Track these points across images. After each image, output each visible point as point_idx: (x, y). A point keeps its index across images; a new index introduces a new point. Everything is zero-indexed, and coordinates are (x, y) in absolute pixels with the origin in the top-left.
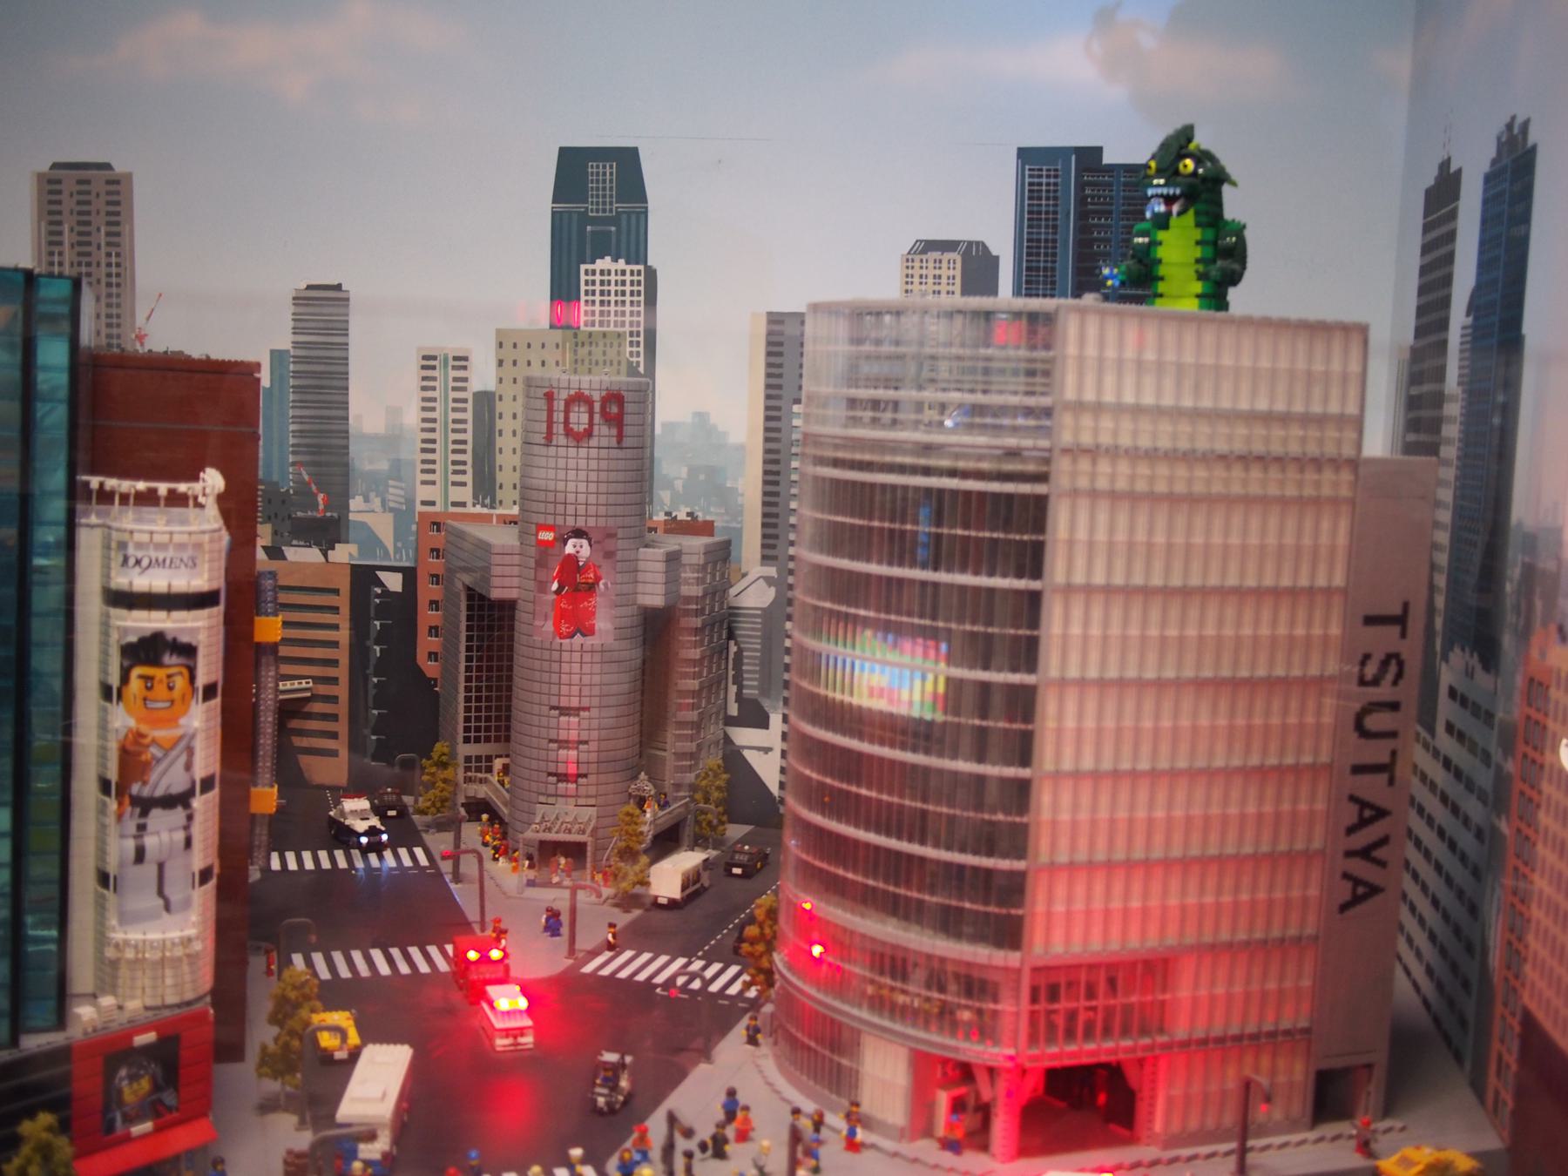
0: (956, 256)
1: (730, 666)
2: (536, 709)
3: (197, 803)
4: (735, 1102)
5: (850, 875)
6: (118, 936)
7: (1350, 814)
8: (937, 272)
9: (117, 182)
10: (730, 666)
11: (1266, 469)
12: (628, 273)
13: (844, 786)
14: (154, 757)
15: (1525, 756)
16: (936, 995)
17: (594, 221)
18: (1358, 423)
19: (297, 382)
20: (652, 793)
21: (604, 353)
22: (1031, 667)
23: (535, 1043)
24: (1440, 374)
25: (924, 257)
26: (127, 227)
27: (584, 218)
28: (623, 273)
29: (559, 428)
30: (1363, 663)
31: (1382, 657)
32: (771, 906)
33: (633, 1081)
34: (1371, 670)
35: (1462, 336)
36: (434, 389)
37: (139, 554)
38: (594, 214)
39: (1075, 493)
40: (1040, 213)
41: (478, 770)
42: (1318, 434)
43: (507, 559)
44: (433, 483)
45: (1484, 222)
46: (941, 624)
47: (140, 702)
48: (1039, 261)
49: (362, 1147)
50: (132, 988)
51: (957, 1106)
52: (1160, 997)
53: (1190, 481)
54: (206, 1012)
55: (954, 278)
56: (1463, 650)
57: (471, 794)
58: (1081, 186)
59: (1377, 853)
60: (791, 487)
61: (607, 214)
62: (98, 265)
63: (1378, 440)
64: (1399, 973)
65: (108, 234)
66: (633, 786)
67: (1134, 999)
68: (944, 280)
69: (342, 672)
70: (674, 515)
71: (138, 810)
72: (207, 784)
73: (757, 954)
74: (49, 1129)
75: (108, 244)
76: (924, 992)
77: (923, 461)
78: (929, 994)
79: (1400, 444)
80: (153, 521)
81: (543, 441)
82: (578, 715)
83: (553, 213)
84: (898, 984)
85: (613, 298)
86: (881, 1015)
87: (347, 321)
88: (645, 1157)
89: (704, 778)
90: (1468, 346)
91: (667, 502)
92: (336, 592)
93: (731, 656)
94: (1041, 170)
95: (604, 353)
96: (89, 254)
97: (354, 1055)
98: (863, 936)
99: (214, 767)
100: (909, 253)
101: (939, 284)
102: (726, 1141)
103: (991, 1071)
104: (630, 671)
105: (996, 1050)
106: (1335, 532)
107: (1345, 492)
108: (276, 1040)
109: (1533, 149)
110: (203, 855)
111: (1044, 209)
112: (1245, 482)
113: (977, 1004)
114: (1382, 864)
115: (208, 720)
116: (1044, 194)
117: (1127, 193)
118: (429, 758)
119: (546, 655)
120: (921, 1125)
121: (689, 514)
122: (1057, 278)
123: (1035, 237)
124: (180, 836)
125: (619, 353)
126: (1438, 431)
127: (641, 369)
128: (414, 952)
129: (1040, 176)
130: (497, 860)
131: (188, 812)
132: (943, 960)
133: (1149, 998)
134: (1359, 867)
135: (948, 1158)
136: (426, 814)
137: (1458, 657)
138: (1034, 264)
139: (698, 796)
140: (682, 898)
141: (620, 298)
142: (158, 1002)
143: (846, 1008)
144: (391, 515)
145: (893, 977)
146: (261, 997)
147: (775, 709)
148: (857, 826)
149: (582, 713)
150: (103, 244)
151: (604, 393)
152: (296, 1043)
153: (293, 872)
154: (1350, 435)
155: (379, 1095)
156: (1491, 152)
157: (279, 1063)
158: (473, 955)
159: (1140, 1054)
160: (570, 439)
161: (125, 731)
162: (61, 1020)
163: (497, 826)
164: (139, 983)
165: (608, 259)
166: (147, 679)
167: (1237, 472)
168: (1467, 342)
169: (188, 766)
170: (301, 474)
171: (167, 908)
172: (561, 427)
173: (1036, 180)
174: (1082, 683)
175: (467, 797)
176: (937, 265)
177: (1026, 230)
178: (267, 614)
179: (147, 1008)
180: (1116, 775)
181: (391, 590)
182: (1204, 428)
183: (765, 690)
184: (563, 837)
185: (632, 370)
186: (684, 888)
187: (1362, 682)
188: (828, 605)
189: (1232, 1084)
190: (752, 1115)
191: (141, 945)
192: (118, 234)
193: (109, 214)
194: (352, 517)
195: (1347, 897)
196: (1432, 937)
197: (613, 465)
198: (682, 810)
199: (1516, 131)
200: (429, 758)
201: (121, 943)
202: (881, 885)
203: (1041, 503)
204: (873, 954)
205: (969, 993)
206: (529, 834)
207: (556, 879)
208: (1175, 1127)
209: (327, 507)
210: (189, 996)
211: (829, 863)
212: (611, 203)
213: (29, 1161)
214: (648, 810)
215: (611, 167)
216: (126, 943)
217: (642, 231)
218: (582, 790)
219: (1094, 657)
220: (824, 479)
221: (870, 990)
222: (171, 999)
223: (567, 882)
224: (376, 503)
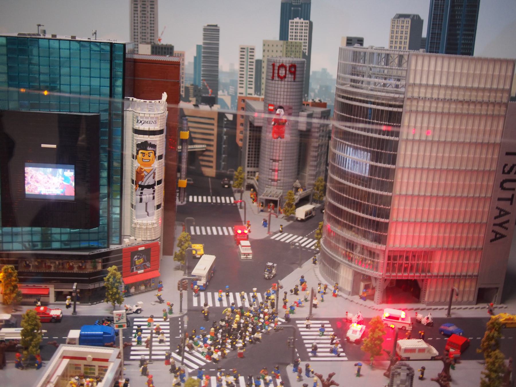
0: (409, 20)
3: (156, 187)
6: (136, 221)
8: (403, 25)
17: (294, 6)
22: (394, 163)
28: (302, 23)
29: (276, 75)
30: (504, 167)
31: (512, 165)
34: (507, 169)
41: (251, 175)
43: (259, 121)
44: (242, 87)
47: (141, 160)
49: (198, 282)
51: (367, 287)
52: (429, 262)
59: (506, 225)
65: (151, 8)
68: (405, 27)
69: (214, 143)
72: (159, 182)
74: (115, 270)
85: (299, 31)
91: (313, 96)
92: (213, 119)
96: (145, 14)
102: (298, 290)
103: (376, 279)
114: (506, 229)
118: (237, 171)
120: (355, 291)
124: (152, 196)
125: (300, 49)
127: (307, 54)
135: (361, 301)
139: (315, 188)
143: (337, 256)
157: (180, 258)
158: (239, 232)
165: (298, 18)
167: (466, 106)
169: (154, 178)
171: (148, 215)
185: (304, 55)
186: (306, 216)
190: (307, 284)
194: (219, 97)
197: (292, 87)
200: (237, 171)
202: (348, 223)
205: (370, 256)
206: (261, 197)
208: (431, 300)
209: (212, 93)
210: (154, 238)
213: (110, 278)
218: (279, 184)
220: (340, 102)
224: (226, 93)
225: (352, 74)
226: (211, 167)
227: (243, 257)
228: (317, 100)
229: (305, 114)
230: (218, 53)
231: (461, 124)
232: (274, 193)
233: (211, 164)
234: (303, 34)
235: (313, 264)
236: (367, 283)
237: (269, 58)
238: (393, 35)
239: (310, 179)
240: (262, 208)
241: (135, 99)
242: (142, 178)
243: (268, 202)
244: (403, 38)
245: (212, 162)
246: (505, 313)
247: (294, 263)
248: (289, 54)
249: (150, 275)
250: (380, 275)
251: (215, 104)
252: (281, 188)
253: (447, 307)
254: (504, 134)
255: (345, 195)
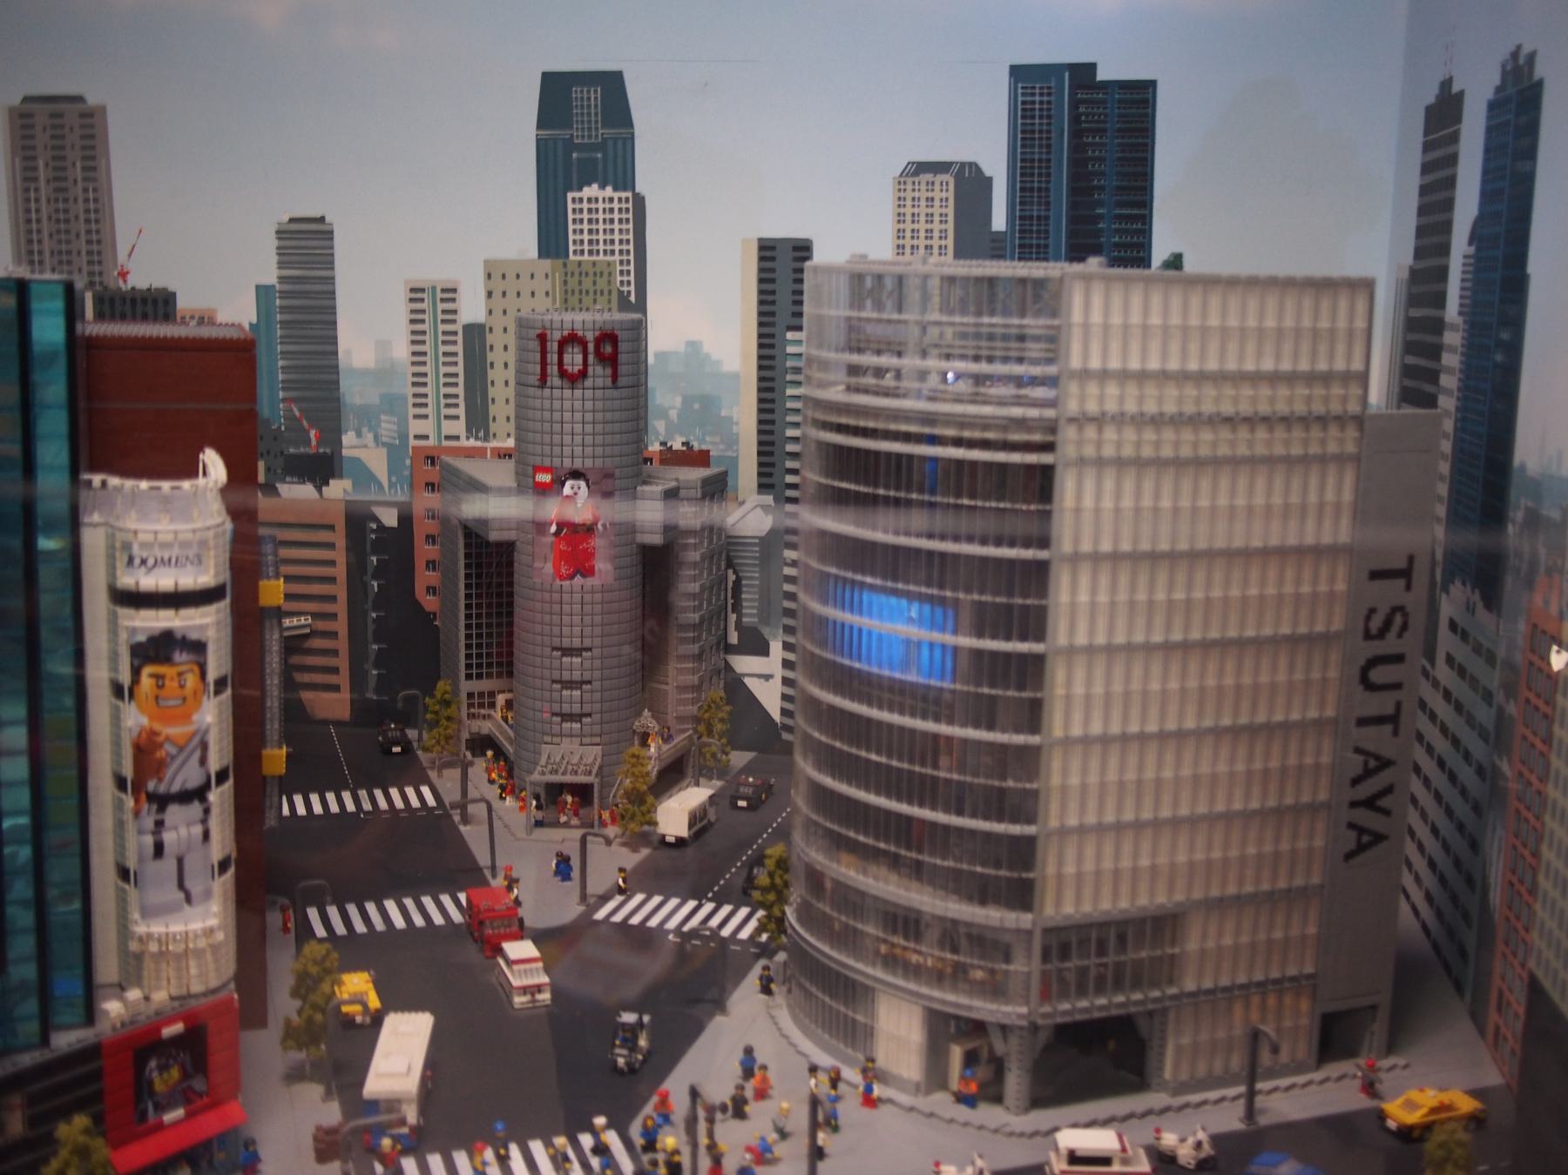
0: (948, 178)
1: (729, 595)
2: (538, 650)
3: (213, 797)
4: (753, 1060)
5: (861, 838)
6: (141, 929)
7: (1356, 764)
8: (930, 194)
9: (91, 115)
10: (729, 595)
11: (1271, 430)
12: (616, 200)
13: (854, 751)
14: (168, 754)
15: (1528, 701)
16: (949, 956)
18: (1363, 378)
19: (287, 317)
20: (656, 729)
21: (595, 283)
23: (553, 999)
24: (1440, 300)
25: (917, 179)
26: (104, 161)
27: (569, 145)
28: (611, 200)
29: (553, 369)
30: (1368, 618)
32: (781, 857)
33: (651, 1040)
34: (1376, 623)
35: (1464, 265)
36: (423, 321)
37: (145, 555)
38: (580, 141)
39: (1082, 462)
40: (1033, 132)
41: (481, 706)
42: (1323, 392)
44: (426, 417)
45: (1488, 151)
46: (949, 594)
48: (1033, 153)
50: (158, 978)
51: (970, 1059)
52: (1169, 951)
53: (1195, 445)
54: (233, 998)
55: (947, 199)
56: (1464, 584)
57: (475, 729)
58: (1075, 104)
59: (1384, 802)
60: (786, 415)
61: (593, 141)
62: (76, 200)
63: (1378, 392)
64: (1404, 907)
65: (84, 169)
66: (637, 723)
67: (1144, 954)
68: (937, 203)
69: (341, 608)
70: (669, 445)
71: (155, 807)
72: (222, 777)
73: (768, 903)
74: (86, 1131)
75: (85, 179)
76: (937, 953)
77: (927, 430)
78: (943, 955)
79: (1397, 390)
80: (158, 521)
81: (537, 383)
82: (581, 655)
83: (538, 141)
84: (912, 945)
85: (601, 227)
86: (894, 974)
87: (332, 255)
88: (666, 1118)
89: (706, 711)
90: (1471, 269)
91: (663, 432)
92: (331, 527)
93: (730, 585)
94: (1034, 88)
95: (595, 283)
97: (377, 1020)
98: (876, 898)
99: (228, 759)
100: (901, 175)
101: (932, 206)
102: (745, 1102)
103: (1004, 1029)
104: (632, 588)
105: (1008, 1009)
106: (1341, 488)
107: (1350, 448)
108: (300, 1013)
109: (1540, 83)
110: (222, 842)
111: (1037, 128)
112: (1250, 444)
113: (990, 965)
114: (1386, 812)
115: (220, 713)
116: (1037, 113)
117: (1122, 111)
118: (433, 696)
119: (547, 596)
120: (935, 1077)
121: (683, 444)
122: (1052, 199)
123: (1028, 157)
124: (197, 830)
126: (1438, 358)
127: (632, 298)
128: (427, 901)
129: (1033, 95)
130: (505, 799)
131: (205, 805)
132: (955, 922)
133: (1159, 952)
134: (1365, 817)
135: (963, 1112)
136: (432, 752)
137: (1457, 589)
138: (1028, 185)
139: (702, 728)
140: (690, 836)
141: (608, 227)
142: (184, 992)
143: (860, 966)
144: (384, 451)
145: (906, 938)
146: (283, 967)
147: (775, 637)
148: (867, 789)
149: (584, 654)
150: (79, 179)
151: (597, 333)
152: (319, 1017)
153: (302, 817)
154: (1355, 391)
155: (404, 1069)
156: (1495, 79)
159: (1150, 1006)
160: (565, 380)
161: (138, 729)
162: (90, 1014)
163: (502, 763)
164: (164, 974)
165: (595, 186)
166: (158, 677)
168: (1470, 265)
169: (203, 761)
170: (292, 410)
171: (188, 899)
172: (556, 368)
173: (1029, 99)
174: (1090, 650)
175: (470, 733)
176: (930, 187)
177: (1019, 150)
178: (268, 578)
179: (172, 998)
180: (1125, 738)
181: (387, 525)
182: (1210, 391)
183: (765, 615)
184: (569, 778)
186: (691, 826)
187: (1368, 636)
188: (833, 570)
189: (1238, 1031)
191: (164, 937)
192: (94, 169)
193: (83, 148)
194: (345, 452)
195: (1352, 845)
196: (1432, 864)
198: (686, 742)
199: (1521, 61)
200: (433, 696)
201: (144, 937)
203: (1047, 472)
204: (886, 913)
206: (536, 777)
207: (563, 819)
210: (214, 983)
211: (840, 824)
212: (597, 129)
213: (67, 1164)
214: (653, 745)
215: (596, 91)
216: (150, 936)
217: (629, 157)
219: (1102, 623)
221: (883, 949)
222: (197, 988)
223: (575, 821)
225: (851, 350)
226: (336, 688)
227: (519, 1000)
228: (677, 445)
229: (658, 489)
230: (334, 307)
231: (1233, 493)
232: (575, 760)
233: (332, 679)
234: (617, 237)
235: (763, 997)
236: (970, 1046)
237: (523, 314)
238: (901, 226)
239: (681, 702)
240: (540, 815)
241: (114, 481)
242: (159, 768)
243: (554, 792)
244: (936, 234)
245: (335, 670)
246: (1422, 1090)
247: (698, 1001)
248: (573, 300)
249: (209, 1124)
250: (1020, 1016)
251: (333, 476)
252: (597, 740)
253: (1242, 1089)
254: (1360, 513)
255: (874, 757)
